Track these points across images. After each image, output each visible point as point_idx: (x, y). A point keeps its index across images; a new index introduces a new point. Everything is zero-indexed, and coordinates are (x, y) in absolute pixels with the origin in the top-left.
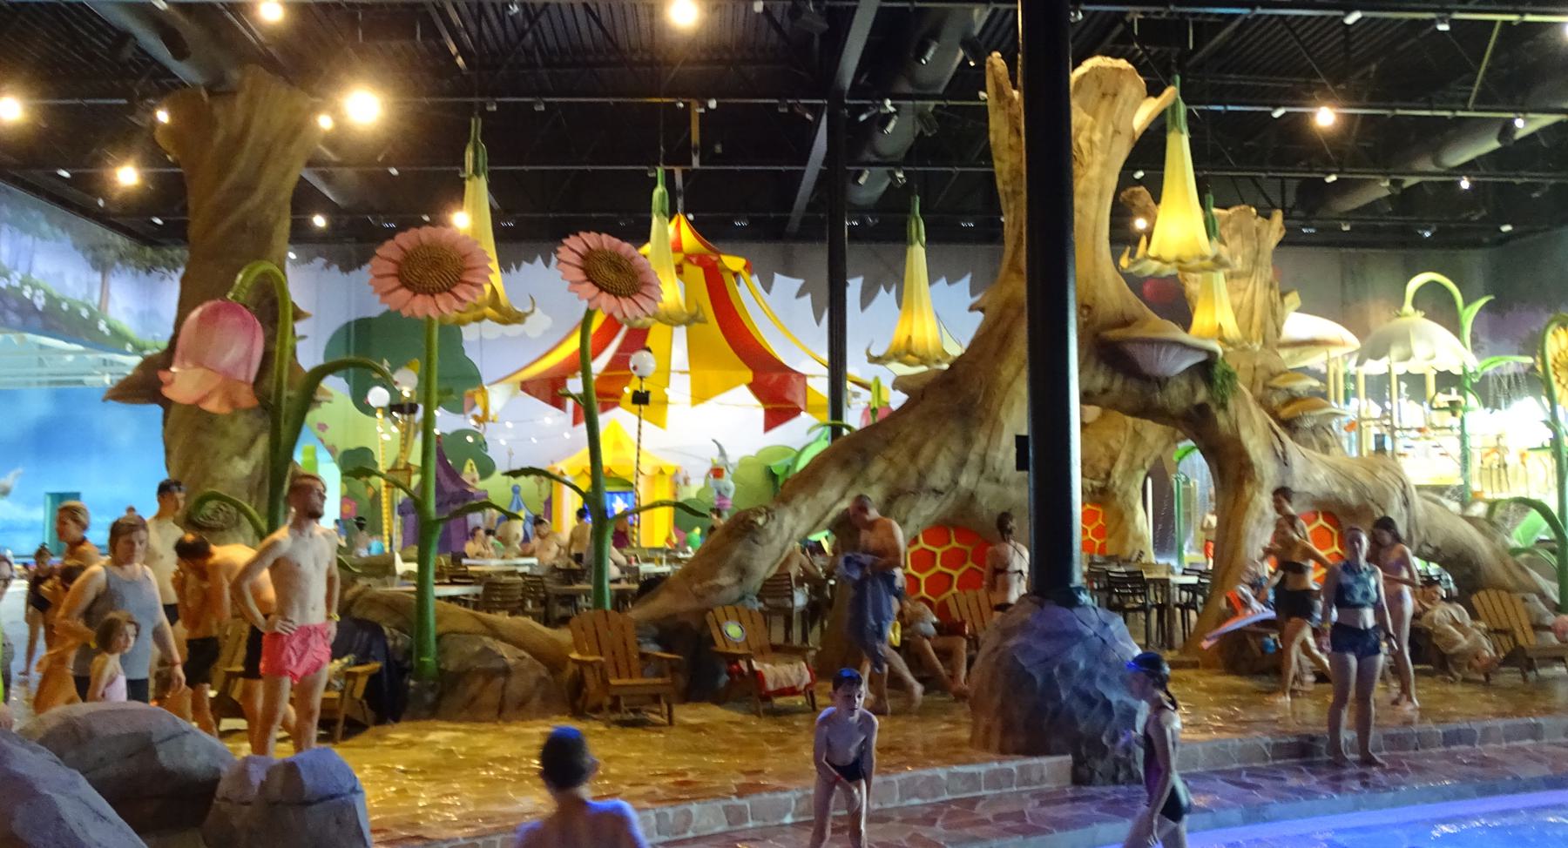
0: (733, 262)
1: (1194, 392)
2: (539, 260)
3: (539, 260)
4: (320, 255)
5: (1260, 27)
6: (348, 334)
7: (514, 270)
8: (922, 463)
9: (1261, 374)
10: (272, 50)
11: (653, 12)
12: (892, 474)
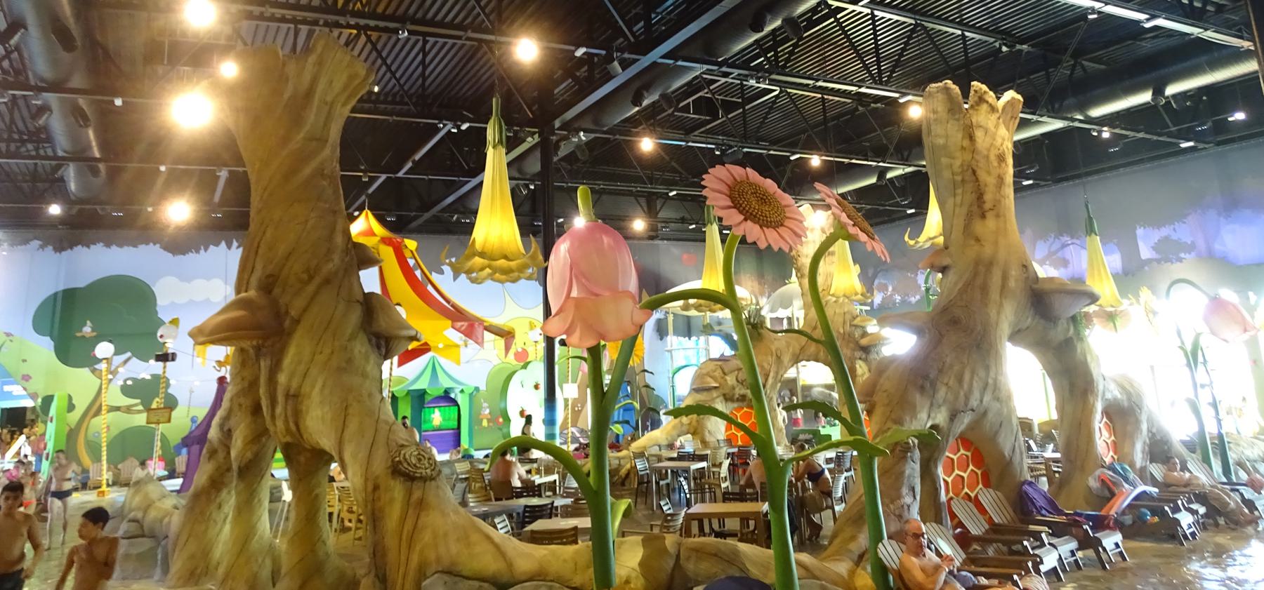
0: (411, 244)
1: (1068, 330)
2: (223, 244)
3: (223, 244)
4: (36, 238)
5: (403, 47)
6: (55, 306)
7: (202, 251)
8: (966, 386)
9: (848, 317)
10: (503, 39)
11: (169, 9)
12: (950, 397)
